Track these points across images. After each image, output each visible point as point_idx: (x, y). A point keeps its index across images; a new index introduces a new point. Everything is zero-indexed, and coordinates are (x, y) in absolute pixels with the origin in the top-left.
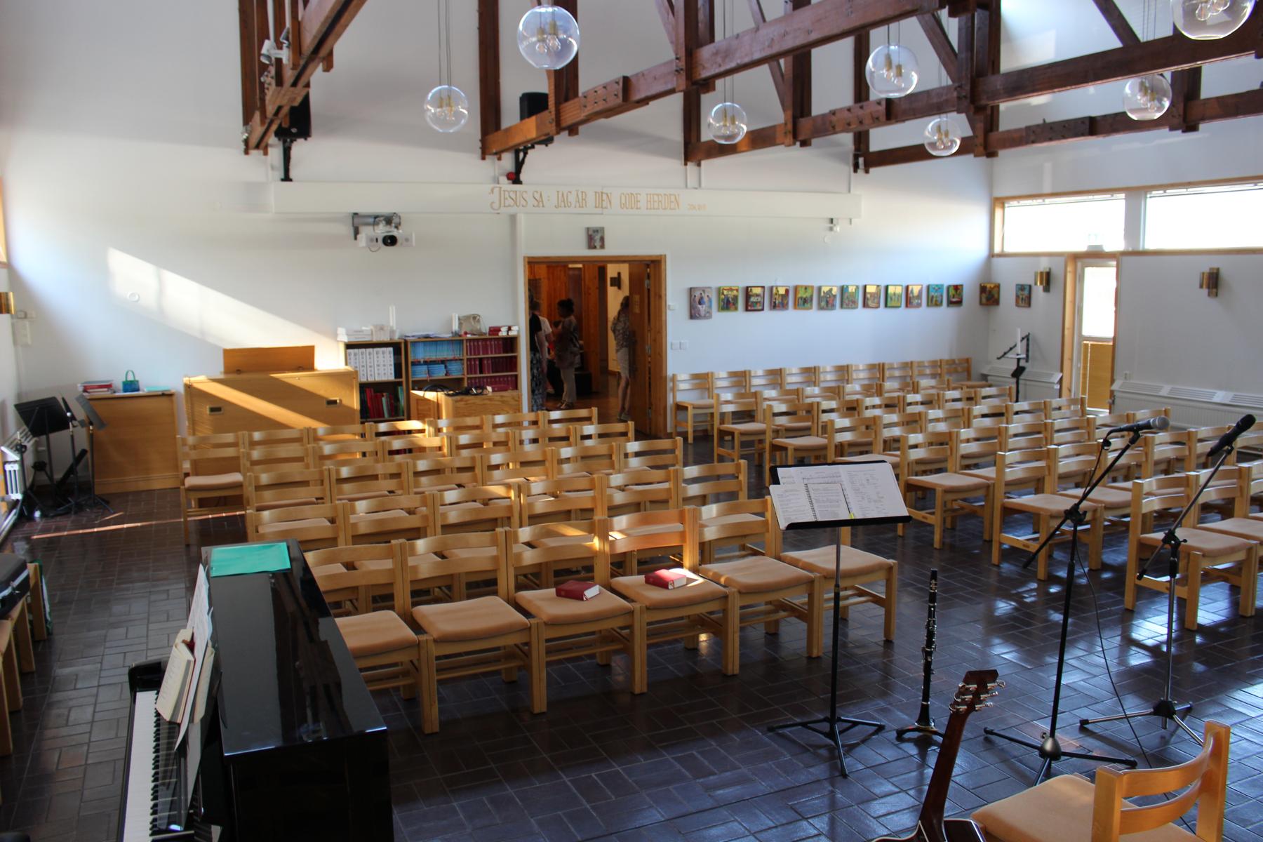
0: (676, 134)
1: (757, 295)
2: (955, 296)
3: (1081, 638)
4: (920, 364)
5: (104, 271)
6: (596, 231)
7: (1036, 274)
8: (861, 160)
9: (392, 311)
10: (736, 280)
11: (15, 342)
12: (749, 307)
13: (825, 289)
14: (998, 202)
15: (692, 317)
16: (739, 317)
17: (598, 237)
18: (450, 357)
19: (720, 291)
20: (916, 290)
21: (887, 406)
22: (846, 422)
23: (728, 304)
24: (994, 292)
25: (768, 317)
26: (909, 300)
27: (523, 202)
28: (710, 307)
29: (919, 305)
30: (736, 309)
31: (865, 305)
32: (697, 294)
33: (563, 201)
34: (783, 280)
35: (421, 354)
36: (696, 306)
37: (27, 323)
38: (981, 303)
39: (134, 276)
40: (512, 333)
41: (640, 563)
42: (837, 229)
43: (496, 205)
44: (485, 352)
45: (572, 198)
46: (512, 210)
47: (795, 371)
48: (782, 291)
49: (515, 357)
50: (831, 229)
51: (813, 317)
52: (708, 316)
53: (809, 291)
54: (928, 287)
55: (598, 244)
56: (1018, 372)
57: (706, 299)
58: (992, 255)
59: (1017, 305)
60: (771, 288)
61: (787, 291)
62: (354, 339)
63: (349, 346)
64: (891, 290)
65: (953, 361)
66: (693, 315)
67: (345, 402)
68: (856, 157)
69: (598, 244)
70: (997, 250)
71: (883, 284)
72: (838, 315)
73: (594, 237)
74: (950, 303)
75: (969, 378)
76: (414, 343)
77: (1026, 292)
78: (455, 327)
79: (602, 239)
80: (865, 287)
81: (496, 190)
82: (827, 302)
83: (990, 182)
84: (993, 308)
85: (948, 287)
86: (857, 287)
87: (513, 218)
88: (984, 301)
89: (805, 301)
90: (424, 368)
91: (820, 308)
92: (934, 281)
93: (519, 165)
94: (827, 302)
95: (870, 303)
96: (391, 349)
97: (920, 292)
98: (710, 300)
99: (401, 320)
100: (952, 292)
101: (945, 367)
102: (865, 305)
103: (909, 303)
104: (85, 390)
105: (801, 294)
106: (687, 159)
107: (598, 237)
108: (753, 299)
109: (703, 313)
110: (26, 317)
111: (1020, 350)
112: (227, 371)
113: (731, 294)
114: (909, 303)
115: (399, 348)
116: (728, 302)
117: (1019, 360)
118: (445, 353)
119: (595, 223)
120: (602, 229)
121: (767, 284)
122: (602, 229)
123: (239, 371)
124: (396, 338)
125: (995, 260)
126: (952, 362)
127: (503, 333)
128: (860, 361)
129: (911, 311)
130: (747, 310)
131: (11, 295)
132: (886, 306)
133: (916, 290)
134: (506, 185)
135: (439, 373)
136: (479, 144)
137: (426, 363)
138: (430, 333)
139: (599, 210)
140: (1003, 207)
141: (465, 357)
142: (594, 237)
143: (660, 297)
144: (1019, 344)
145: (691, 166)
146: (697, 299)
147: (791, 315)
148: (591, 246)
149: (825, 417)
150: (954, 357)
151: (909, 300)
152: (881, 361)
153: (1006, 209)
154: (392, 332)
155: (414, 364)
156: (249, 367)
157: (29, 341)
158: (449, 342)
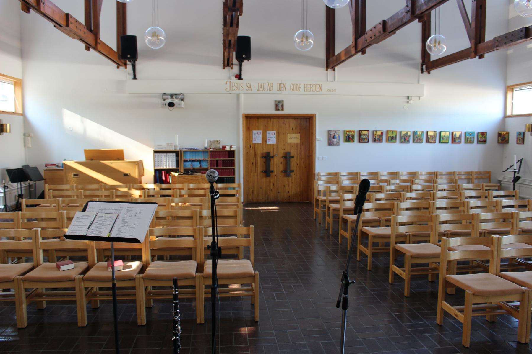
0: (322, 55)
1: (365, 135)
2: (482, 138)
4: (459, 174)
5: (60, 117)
6: (279, 102)
7: (526, 126)
8: (424, 67)
9: (177, 136)
10: (355, 127)
11: (25, 145)
12: (361, 140)
13: (404, 133)
14: (510, 88)
16: (355, 145)
17: (280, 105)
18: (202, 159)
19: (345, 132)
20: (458, 135)
21: (520, 206)
22: (488, 216)
23: (349, 138)
24: (506, 136)
25: (371, 146)
26: (454, 140)
27: (241, 88)
28: (339, 140)
29: (460, 142)
30: (353, 141)
31: (428, 141)
32: (332, 133)
33: (261, 88)
34: (381, 126)
35: (189, 157)
37: (30, 138)
38: (498, 143)
39: (73, 121)
40: (232, 149)
42: (411, 102)
43: (228, 90)
44: (219, 158)
45: (266, 86)
46: (237, 92)
47: (385, 173)
48: (379, 133)
49: (234, 160)
50: (408, 102)
51: (397, 147)
52: (338, 144)
53: (395, 133)
54: (465, 133)
55: (280, 108)
56: (516, 179)
57: (337, 136)
58: (505, 117)
59: (517, 143)
60: (373, 131)
61: (382, 133)
63: (156, 152)
64: (429, 133)
65: (480, 172)
66: (330, 144)
67: (132, 175)
68: (422, 65)
69: (280, 108)
70: (509, 113)
71: (438, 131)
72: (411, 146)
73: (279, 105)
74: (479, 142)
75: (490, 182)
76: (185, 152)
77: (522, 136)
78: (206, 145)
79: (282, 106)
80: (427, 132)
81: (228, 83)
82: (405, 139)
83: (505, 78)
84: (505, 145)
85: (478, 134)
86: (423, 132)
87: (238, 96)
88: (500, 141)
89: (392, 138)
90: (190, 163)
91: (401, 142)
92: (468, 130)
94: (405, 139)
95: (430, 140)
96: (174, 154)
97: (460, 136)
98: (339, 137)
99: (178, 142)
100: (480, 136)
101: (475, 176)
102: (428, 141)
104: (46, 166)
105: (390, 134)
106: (327, 67)
107: (280, 105)
108: (362, 137)
109: (335, 143)
110: (29, 136)
111: (516, 167)
112: (87, 159)
113: (351, 134)
114: (454, 141)
115: (178, 154)
116: (349, 138)
117: (515, 172)
118: (200, 157)
119: (279, 98)
120: (283, 101)
121: (371, 129)
122: (283, 101)
123: (92, 160)
125: (507, 119)
126: (479, 173)
127: (228, 149)
128: (423, 170)
129: (455, 145)
130: (360, 142)
131: (8, 125)
132: (440, 142)
133: (458, 135)
136: (222, 62)
137: (190, 161)
138: (194, 148)
139: (280, 92)
140: (513, 91)
141: (209, 159)
142: (279, 105)
143: (312, 133)
144: (515, 164)
145: (330, 71)
146: (332, 136)
147: (384, 146)
149: (472, 211)
150: (482, 170)
151: (454, 140)
152: (436, 171)
153: (514, 92)
154: (175, 146)
155: (185, 161)
156: (98, 158)
157: (30, 146)
158: (202, 152)
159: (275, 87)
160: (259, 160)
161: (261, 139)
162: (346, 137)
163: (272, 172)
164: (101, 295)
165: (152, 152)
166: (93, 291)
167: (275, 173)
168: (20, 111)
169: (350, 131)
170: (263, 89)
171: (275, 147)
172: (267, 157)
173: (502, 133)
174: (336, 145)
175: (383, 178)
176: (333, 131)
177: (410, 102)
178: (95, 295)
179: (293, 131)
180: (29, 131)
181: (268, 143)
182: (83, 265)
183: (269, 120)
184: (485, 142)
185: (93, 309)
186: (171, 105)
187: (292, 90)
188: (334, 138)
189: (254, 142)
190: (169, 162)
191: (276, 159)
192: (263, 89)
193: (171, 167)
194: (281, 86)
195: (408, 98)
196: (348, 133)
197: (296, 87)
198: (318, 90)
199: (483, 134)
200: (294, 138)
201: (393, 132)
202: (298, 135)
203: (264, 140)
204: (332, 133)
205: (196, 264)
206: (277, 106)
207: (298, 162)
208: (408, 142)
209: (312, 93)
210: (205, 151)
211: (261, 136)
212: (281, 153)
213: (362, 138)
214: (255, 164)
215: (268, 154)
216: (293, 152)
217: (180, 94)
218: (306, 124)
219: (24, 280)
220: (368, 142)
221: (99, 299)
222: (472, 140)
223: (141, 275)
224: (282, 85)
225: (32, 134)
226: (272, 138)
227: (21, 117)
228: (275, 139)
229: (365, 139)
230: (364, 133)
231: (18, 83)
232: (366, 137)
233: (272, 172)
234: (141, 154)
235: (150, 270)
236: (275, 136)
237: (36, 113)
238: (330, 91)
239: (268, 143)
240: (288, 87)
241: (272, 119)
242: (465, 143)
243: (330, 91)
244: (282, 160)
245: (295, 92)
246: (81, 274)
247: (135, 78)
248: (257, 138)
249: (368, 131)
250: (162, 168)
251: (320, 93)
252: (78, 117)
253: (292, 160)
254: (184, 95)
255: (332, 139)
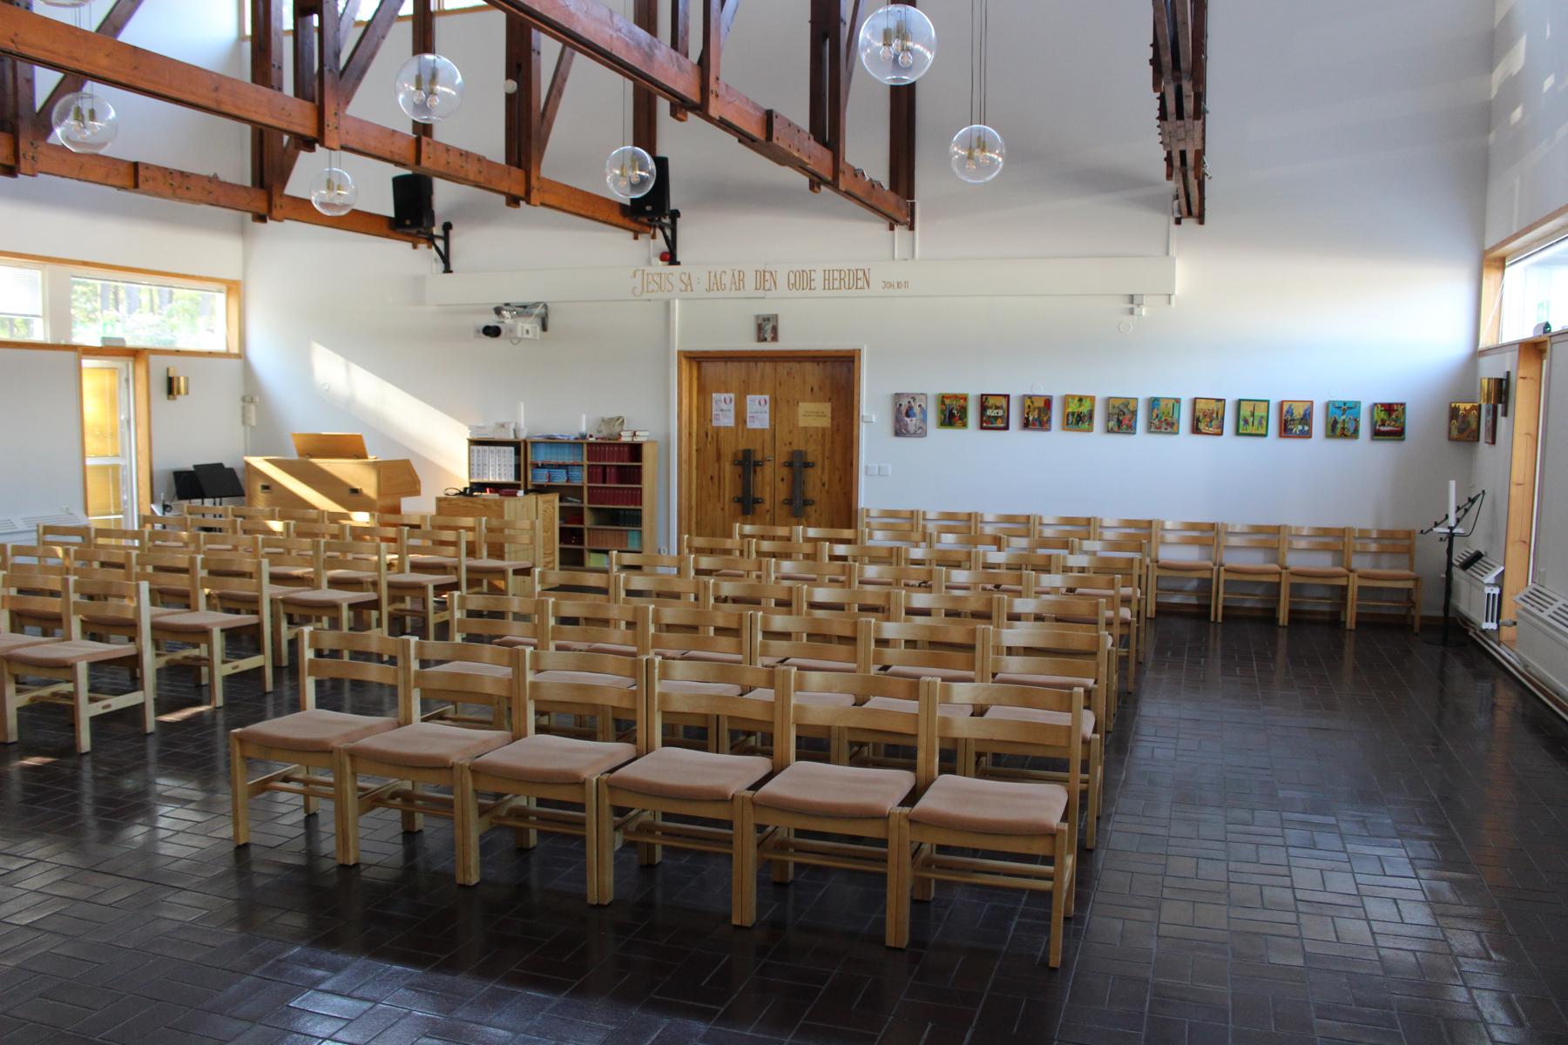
2: (1390, 422)
3: (138, 816)
6: (767, 319)
11: (244, 423)
12: (986, 423)
15: (898, 433)
16: (970, 436)
17: (769, 327)
23: (952, 414)
28: (924, 420)
29: (1307, 435)
30: (965, 425)
32: (905, 403)
33: (716, 284)
35: (543, 456)
36: (904, 418)
37: (253, 407)
38: (1450, 439)
41: (734, 734)
43: (638, 291)
45: (727, 279)
46: (666, 296)
49: (640, 467)
50: (1132, 312)
51: (1097, 442)
52: (921, 432)
55: (769, 335)
57: (917, 410)
62: (476, 437)
64: (1201, 405)
66: (900, 431)
69: (769, 335)
73: (766, 327)
74: (1377, 434)
76: (534, 443)
78: (584, 429)
79: (775, 329)
81: (639, 274)
82: (1121, 418)
83: (1478, 221)
87: (668, 305)
88: (1455, 433)
93: (672, 243)
94: (1120, 422)
95: (1202, 426)
98: (924, 412)
99: (525, 421)
102: (1196, 430)
103: (1285, 430)
107: (769, 327)
108: (989, 412)
109: (912, 429)
110: (252, 401)
115: (518, 446)
116: (951, 415)
118: (566, 457)
119: (767, 310)
120: (776, 317)
122: (776, 317)
124: (522, 436)
126: (1384, 535)
127: (626, 438)
130: (982, 428)
132: (1238, 433)
134: (661, 267)
135: (560, 478)
139: (761, 293)
142: (766, 327)
148: (761, 339)
151: (1293, 423)
152: (1408, 528)
159: (750, 281)
160: (728, 468)
161: (732, 414)
162: (943, 412)
163: (757, 501)
164: (800, 850)
165: (464, 446)
166: (778, 837)
167: (767, 505)
168: (235, 349)
169: (955, 397)
170: (720, 287)
171: (768, 437)
172: (747, 463)
173: (1462, 406)
174: (915, 435)
175: (1048, 532)
176: (908, 395)
177: (1136, 310)
178: (783, 846)
179: (813, 395)
180: (251, 393)
181: (750, 425)
182: (760, 765)
183: (752, 364)
184: (1399, 434)
185: (776, 884)
186: (492, 332)
187: (792, 286)
188: (908, 415)
189: (715, 423)
190: (500, 468)
191: (768, 468)
192: (720, 287)
193: (504, 480)
194: (764, 279)
195: (1132, 298)
196: (947, 402)
197: (802, 280)
198: (860, 284)
199: (1389, 408)
200: (813, 415)
201: (1081, 400)
202: (826, 408)
203: (741, 416)
204: (905, 403)
205: (1064, 799)
206: (760, 328)
207: (826, 478)
208: (1131, 429)
209: (844, 292)
210: (578, 443)
211: (732, 407)
212: (782, 454)
213: (992, 414)
214: (717, 479)
215: (747, 453)
216: (813, 451)
217: (536, 305)
218: (837, 372)
219: (754, 804)
220: (1006, 428)
221: (792, 859)
222: (1350, 426)
223: (906, 810)
224: (768, 276)
225: (257, 399)
226: (759, 413)
227: (237, 363)
228: (767, 416)
229: (996, 418)
230: (991, 401)
231: (234, 288)
232: (1001, 413)
233: (757, 501)
234: (446, 450)
235: (930, 802)
236: (767, 408)
237: (265, 354)
238: (892, 286)
239: (750, 425)
240: (782, 280)
241: (760, 365)
242: (1281, 436)
243: (892, 286)
244: (785, 472)
245: (800, 293)
246: (749, 789)
247: (448, 270)
248: (723, 412)
249: (1007, 396)
250: (485, 480)
251: (866, 292)
252: (340, 360)
253: (810, 471)
254: (545, 306)
255: (904, 418)
